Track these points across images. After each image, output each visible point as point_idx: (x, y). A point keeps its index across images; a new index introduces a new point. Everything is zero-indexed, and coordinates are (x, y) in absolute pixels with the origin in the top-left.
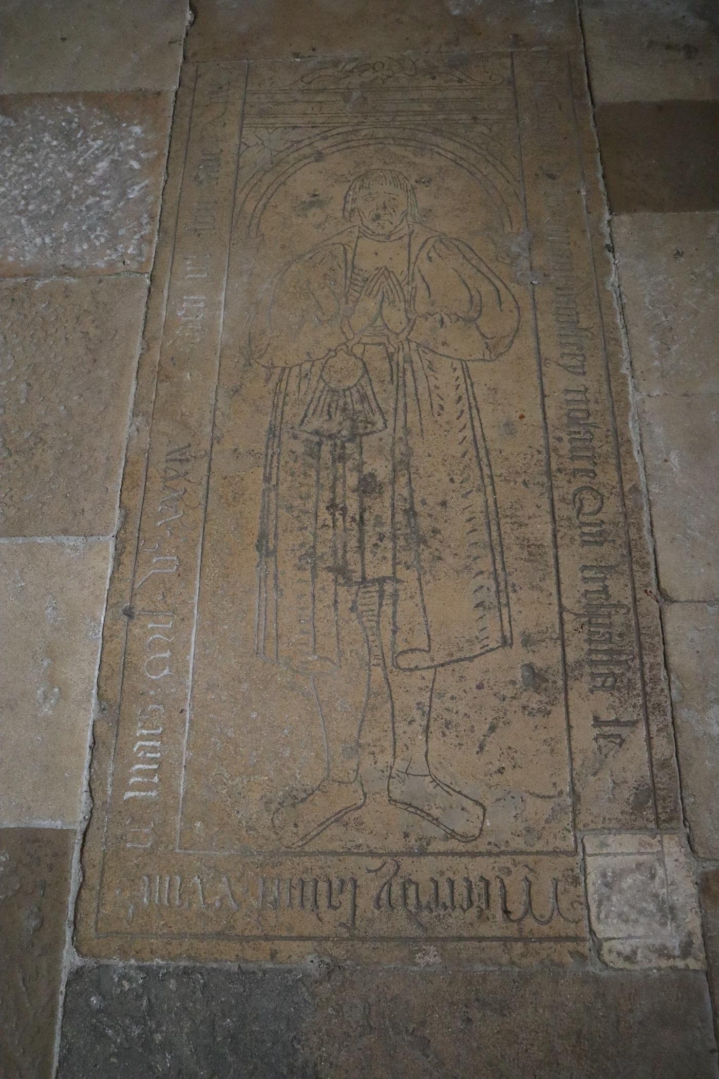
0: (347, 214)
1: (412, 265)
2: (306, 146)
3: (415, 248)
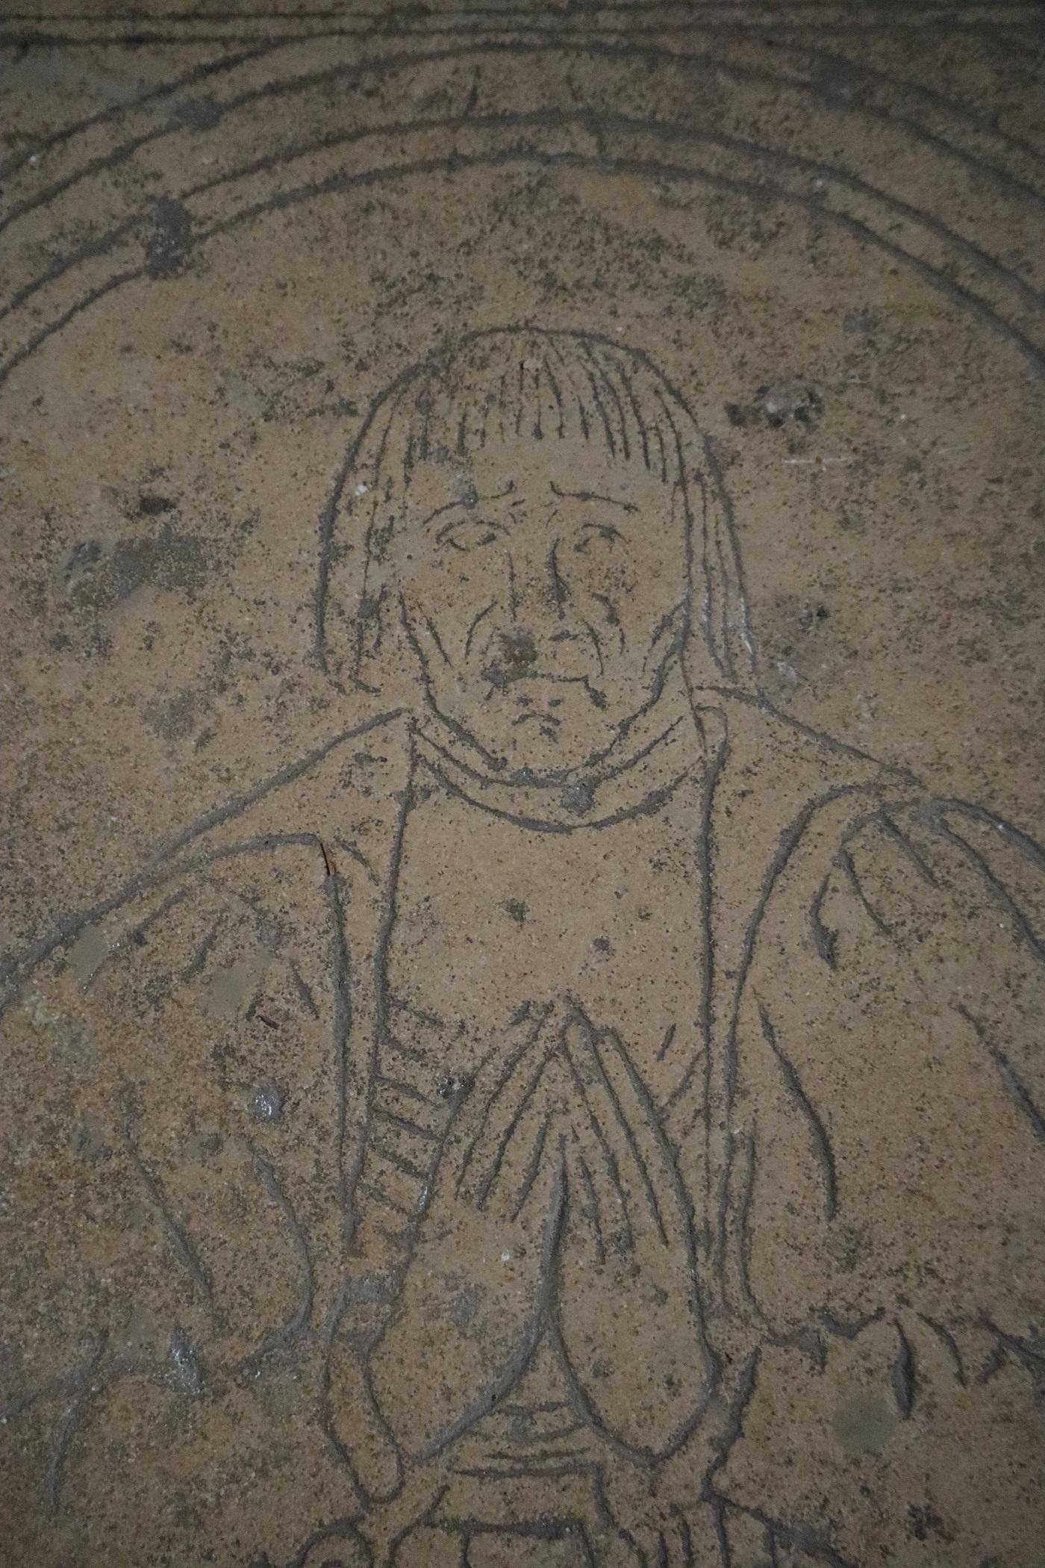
0: (339, 633)
1: (726, 989)
2: (95, 167)
3: (740, 869)
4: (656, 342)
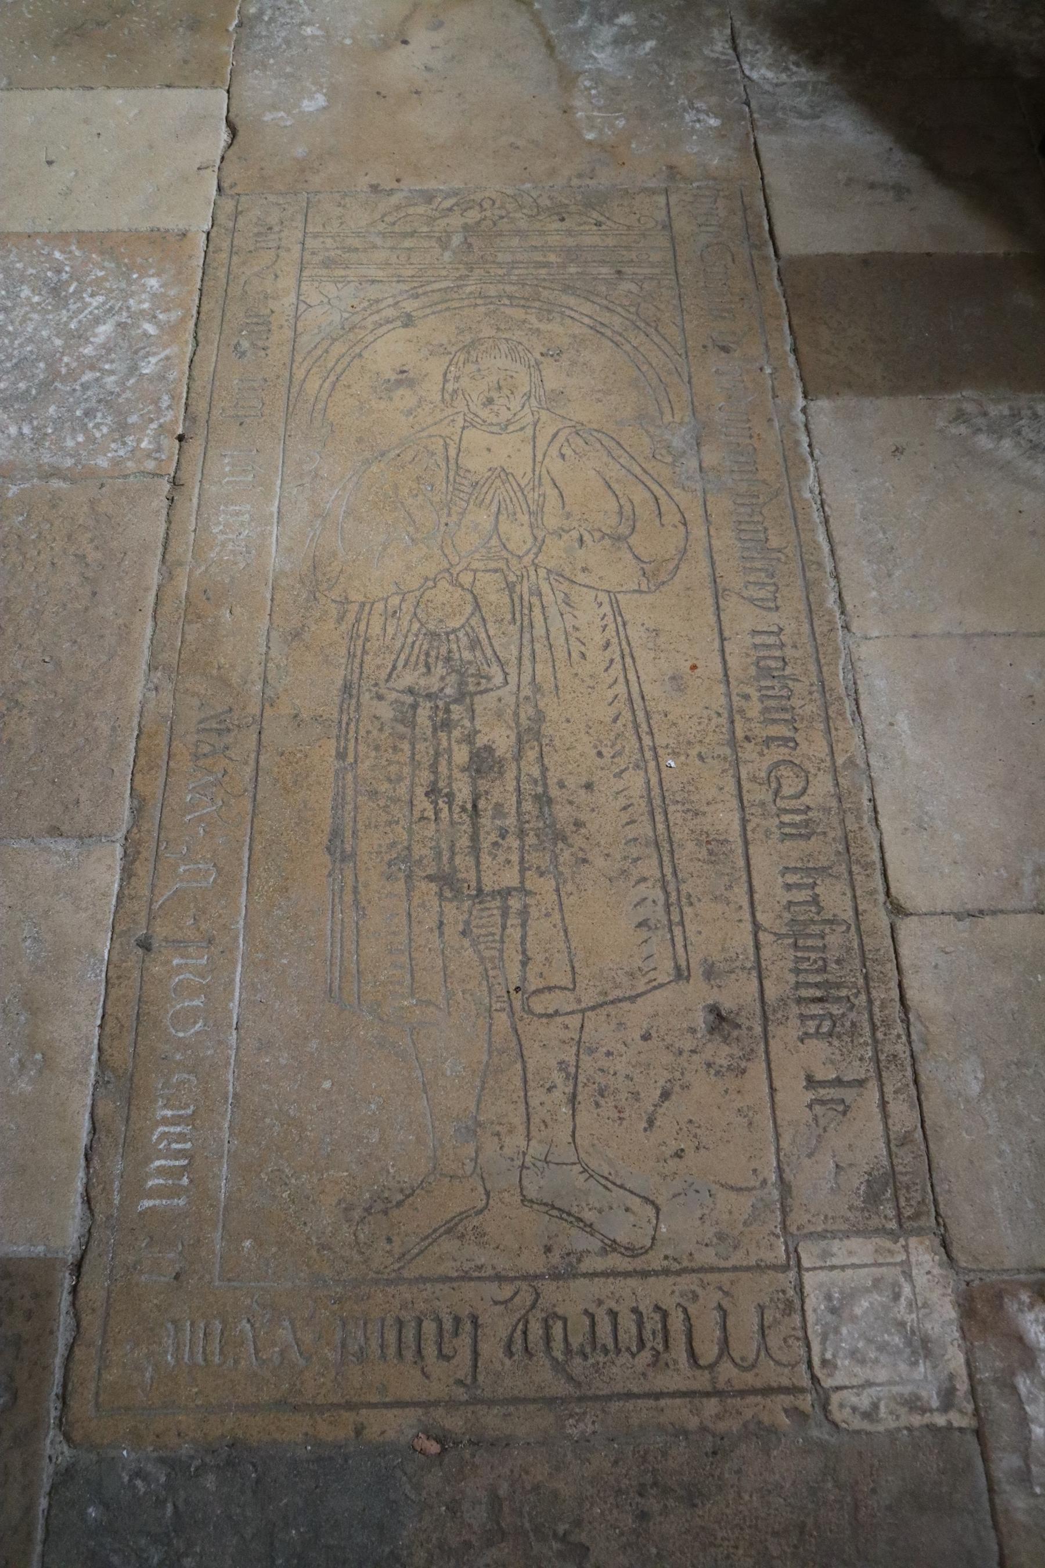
0: (447, 397)
1: (538, 465)
3: (542, 443)
4: (524, 340)
